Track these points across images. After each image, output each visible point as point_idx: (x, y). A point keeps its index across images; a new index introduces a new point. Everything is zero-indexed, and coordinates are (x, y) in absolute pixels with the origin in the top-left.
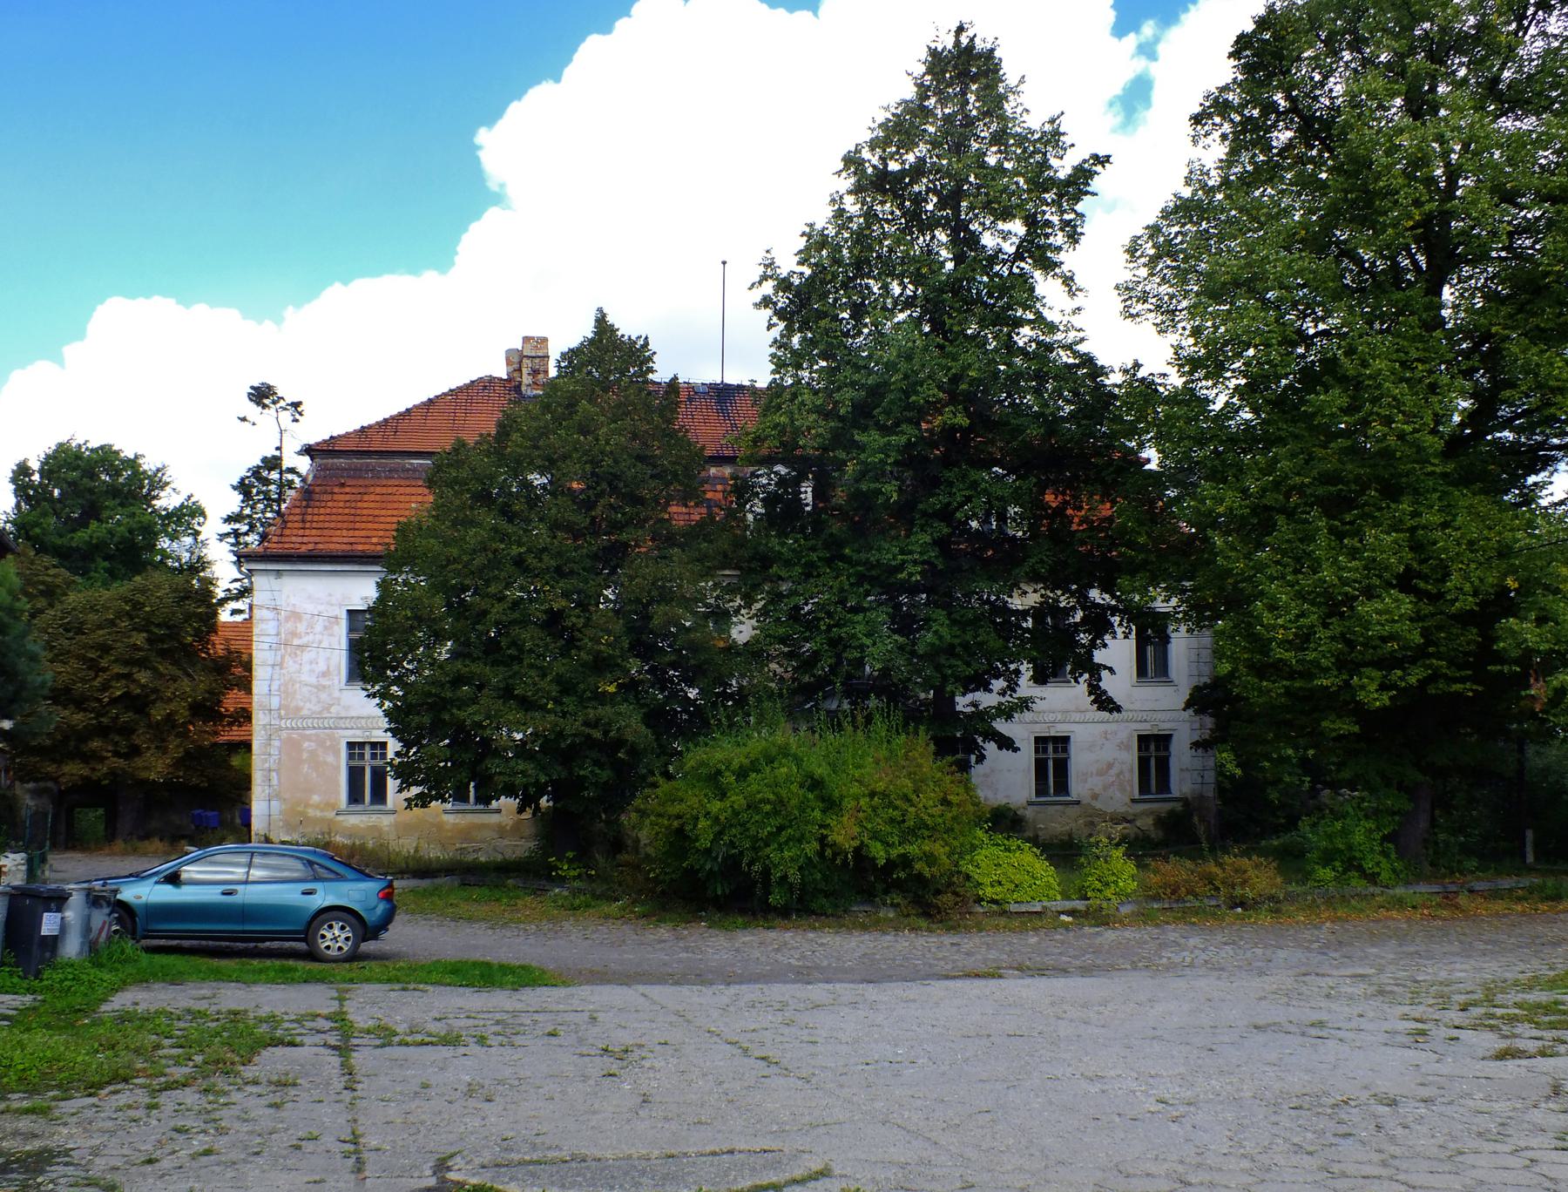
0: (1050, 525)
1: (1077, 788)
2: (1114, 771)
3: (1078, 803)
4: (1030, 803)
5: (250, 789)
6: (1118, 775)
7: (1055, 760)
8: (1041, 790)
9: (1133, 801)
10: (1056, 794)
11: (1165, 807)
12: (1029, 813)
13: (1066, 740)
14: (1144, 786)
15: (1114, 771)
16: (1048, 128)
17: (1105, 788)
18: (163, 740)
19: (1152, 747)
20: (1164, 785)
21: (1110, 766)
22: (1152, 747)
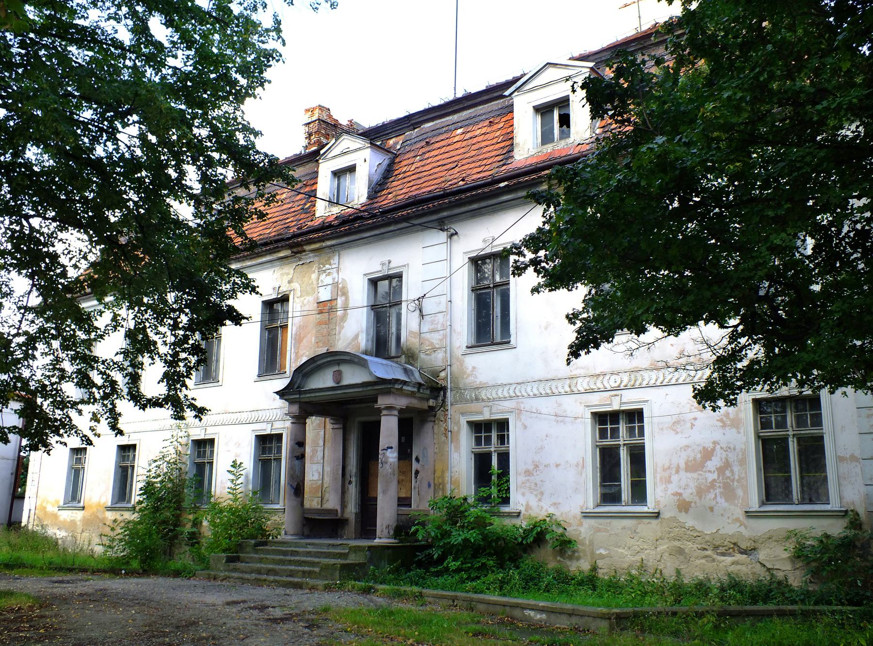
0: (863, 8)
1: (657, 492)
2: (714, 463)
3: (657, 515)
4: (586, 515)
5: (377, 477)
6: (721, 470)
7: (800, 439)
8: (610, 496)
9: (749, 514)
10: (802, 502)
11: (816, 528)
12: (582, 531)
13: (635, 416)
14: (774, 489)
15: (714, 463)
16: (95, 24)
17: (701, 492)
18: (687, 24)
19: (790, 419)
20: (815, 488)
21: (707, 454)
22: (790, 419)
